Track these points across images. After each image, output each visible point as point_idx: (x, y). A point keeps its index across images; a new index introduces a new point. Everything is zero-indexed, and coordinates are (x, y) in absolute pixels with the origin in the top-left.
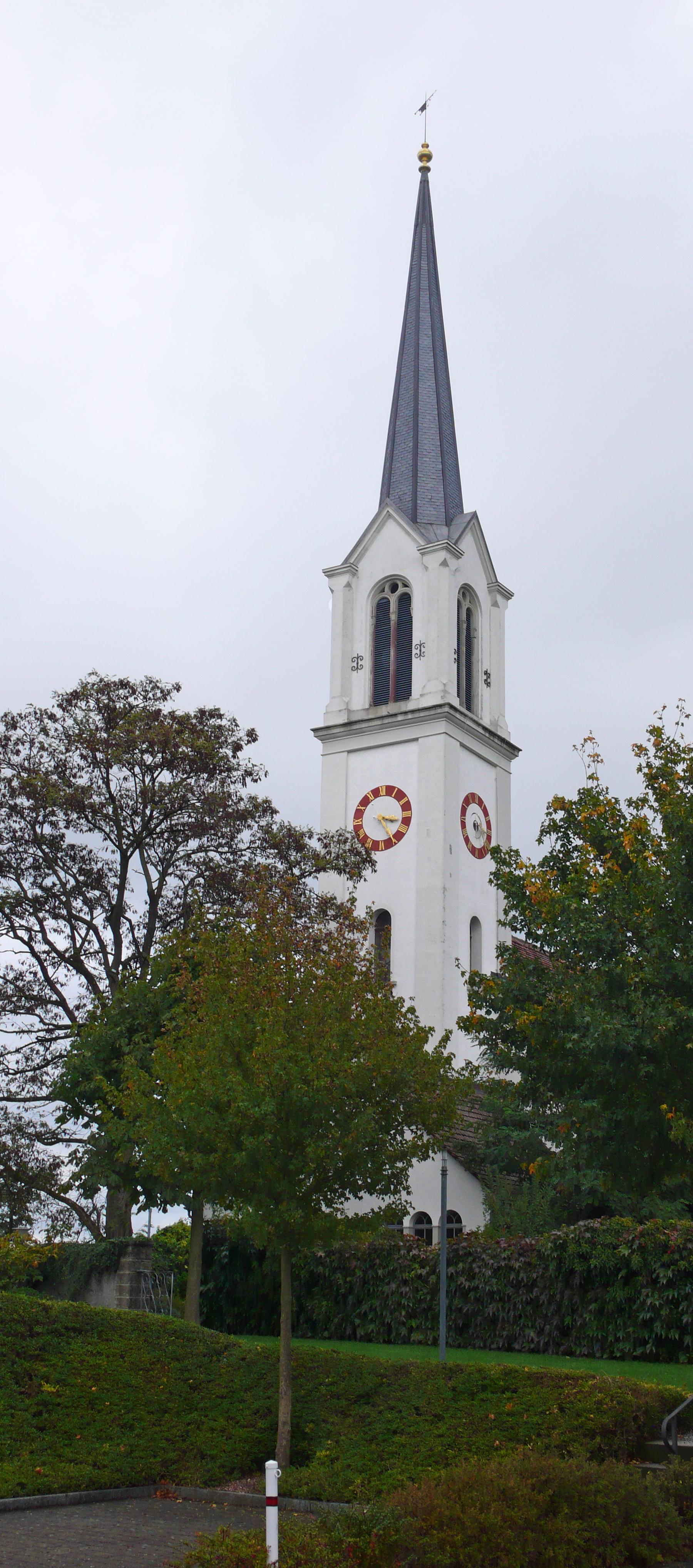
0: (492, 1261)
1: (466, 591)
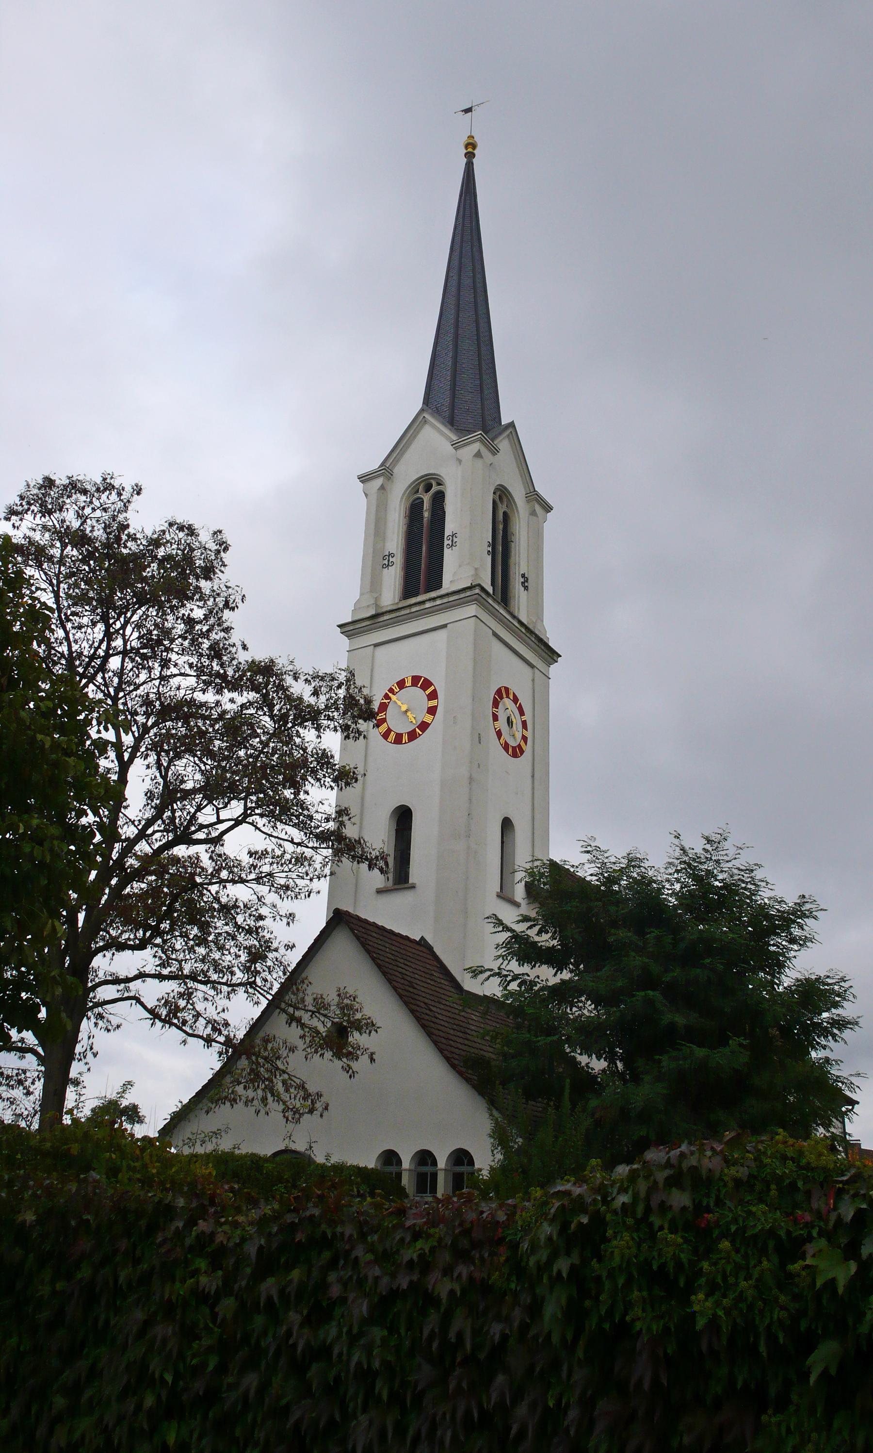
0: (377, 1271)
1: (502, 494)
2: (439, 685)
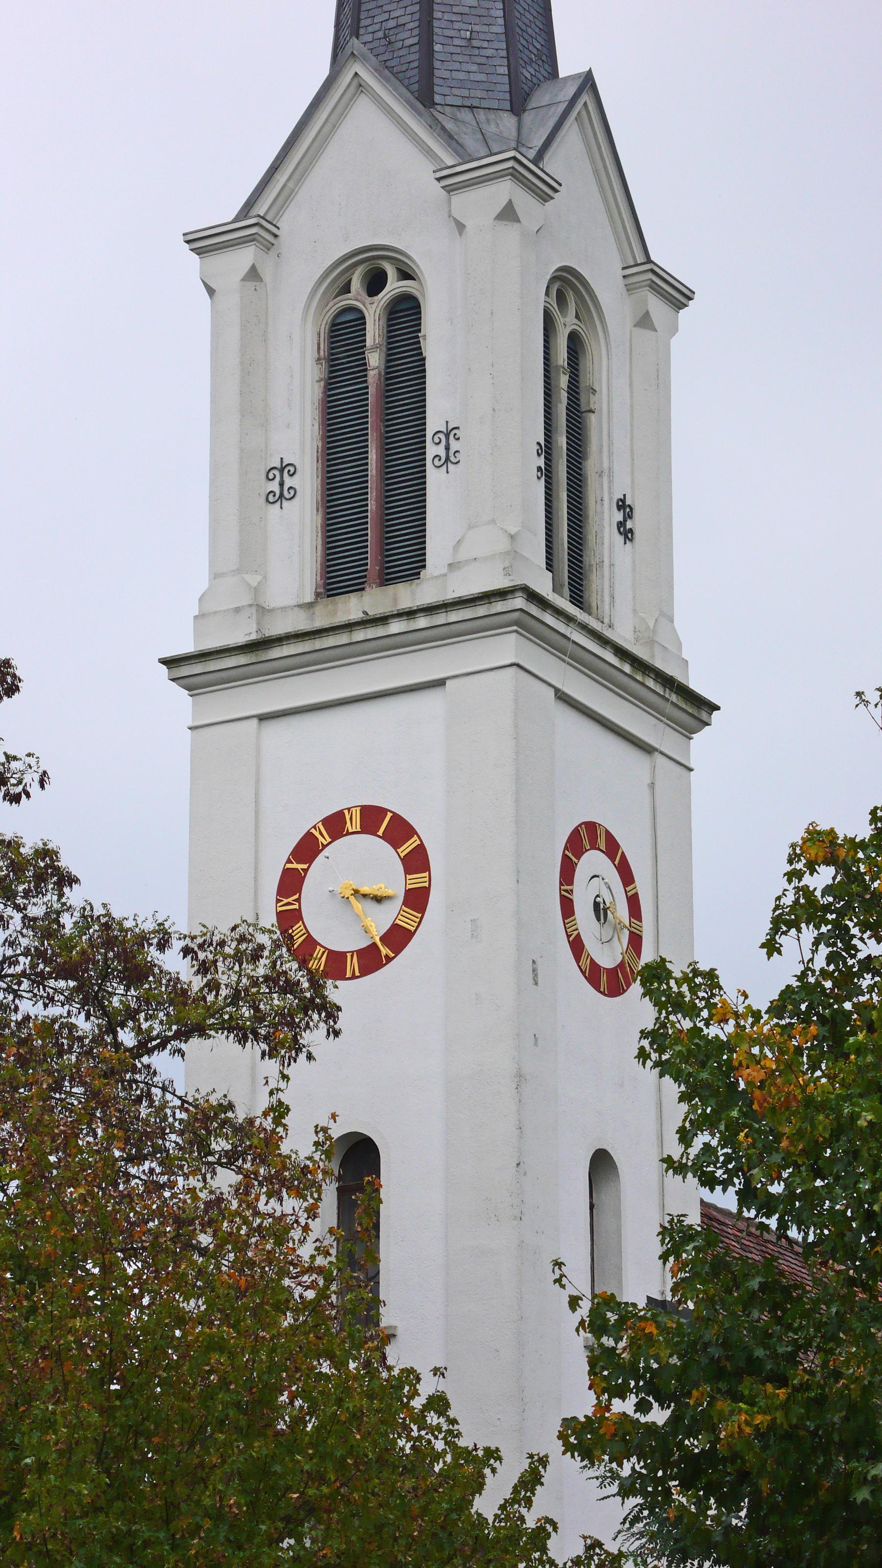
1: (567, 285)
2: (430, 833)
